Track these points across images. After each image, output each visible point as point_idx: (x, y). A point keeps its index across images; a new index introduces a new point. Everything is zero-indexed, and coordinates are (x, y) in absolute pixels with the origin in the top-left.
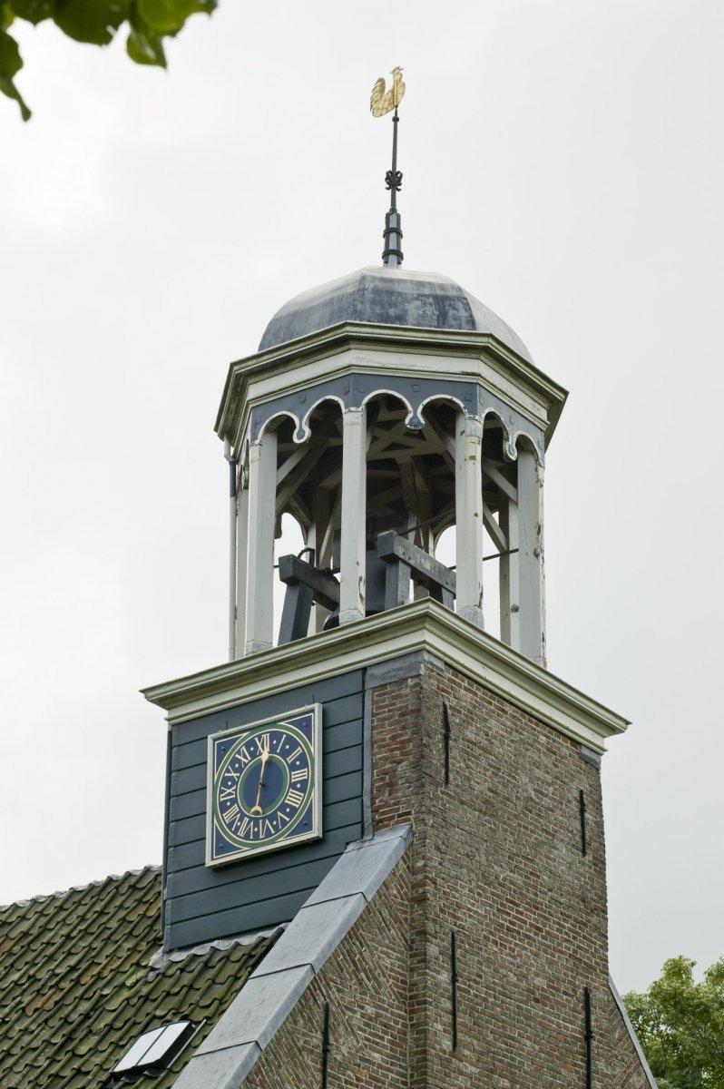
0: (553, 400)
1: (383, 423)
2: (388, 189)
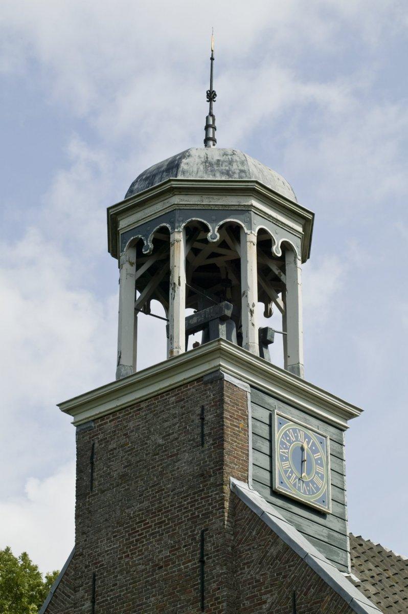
0: (307, 221)
1: (199, 240)
2: (208, 101)
